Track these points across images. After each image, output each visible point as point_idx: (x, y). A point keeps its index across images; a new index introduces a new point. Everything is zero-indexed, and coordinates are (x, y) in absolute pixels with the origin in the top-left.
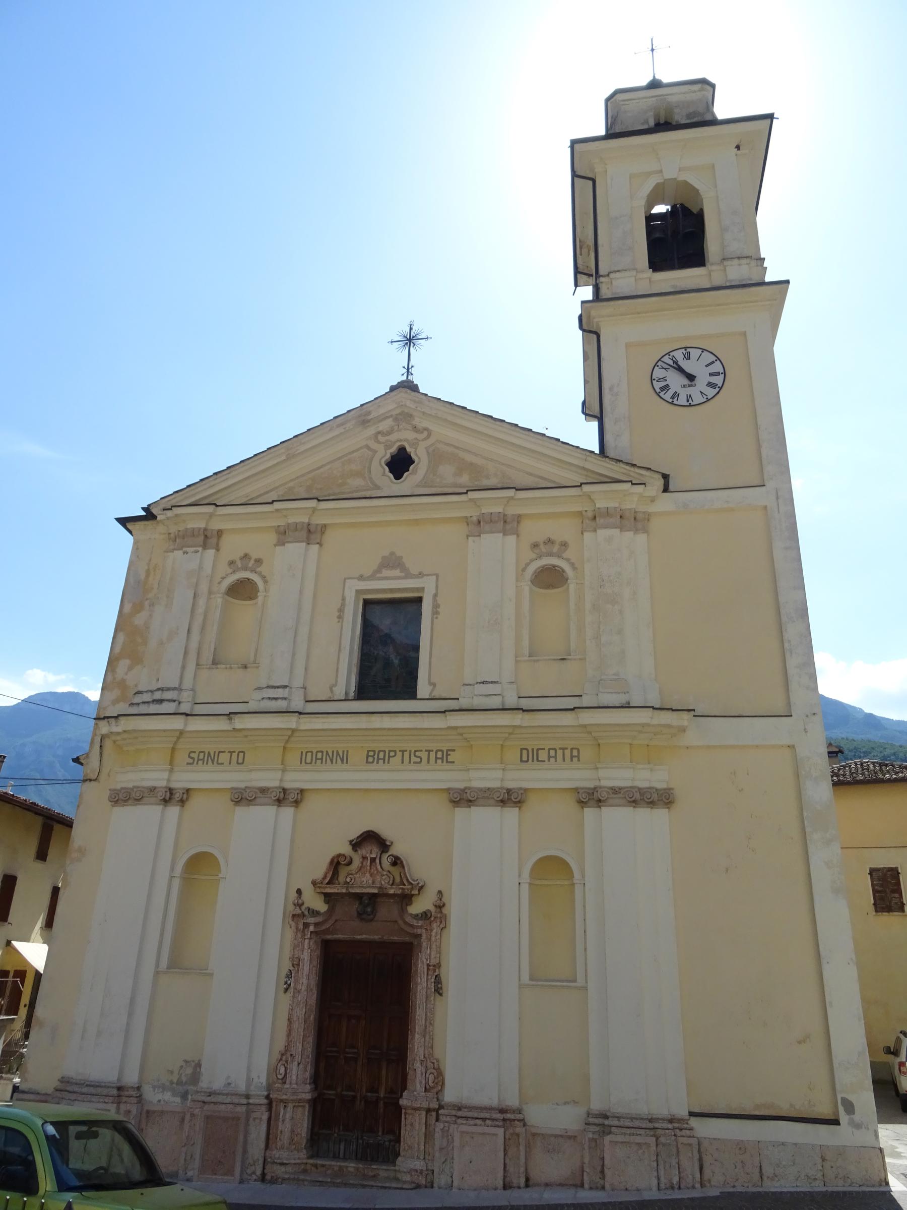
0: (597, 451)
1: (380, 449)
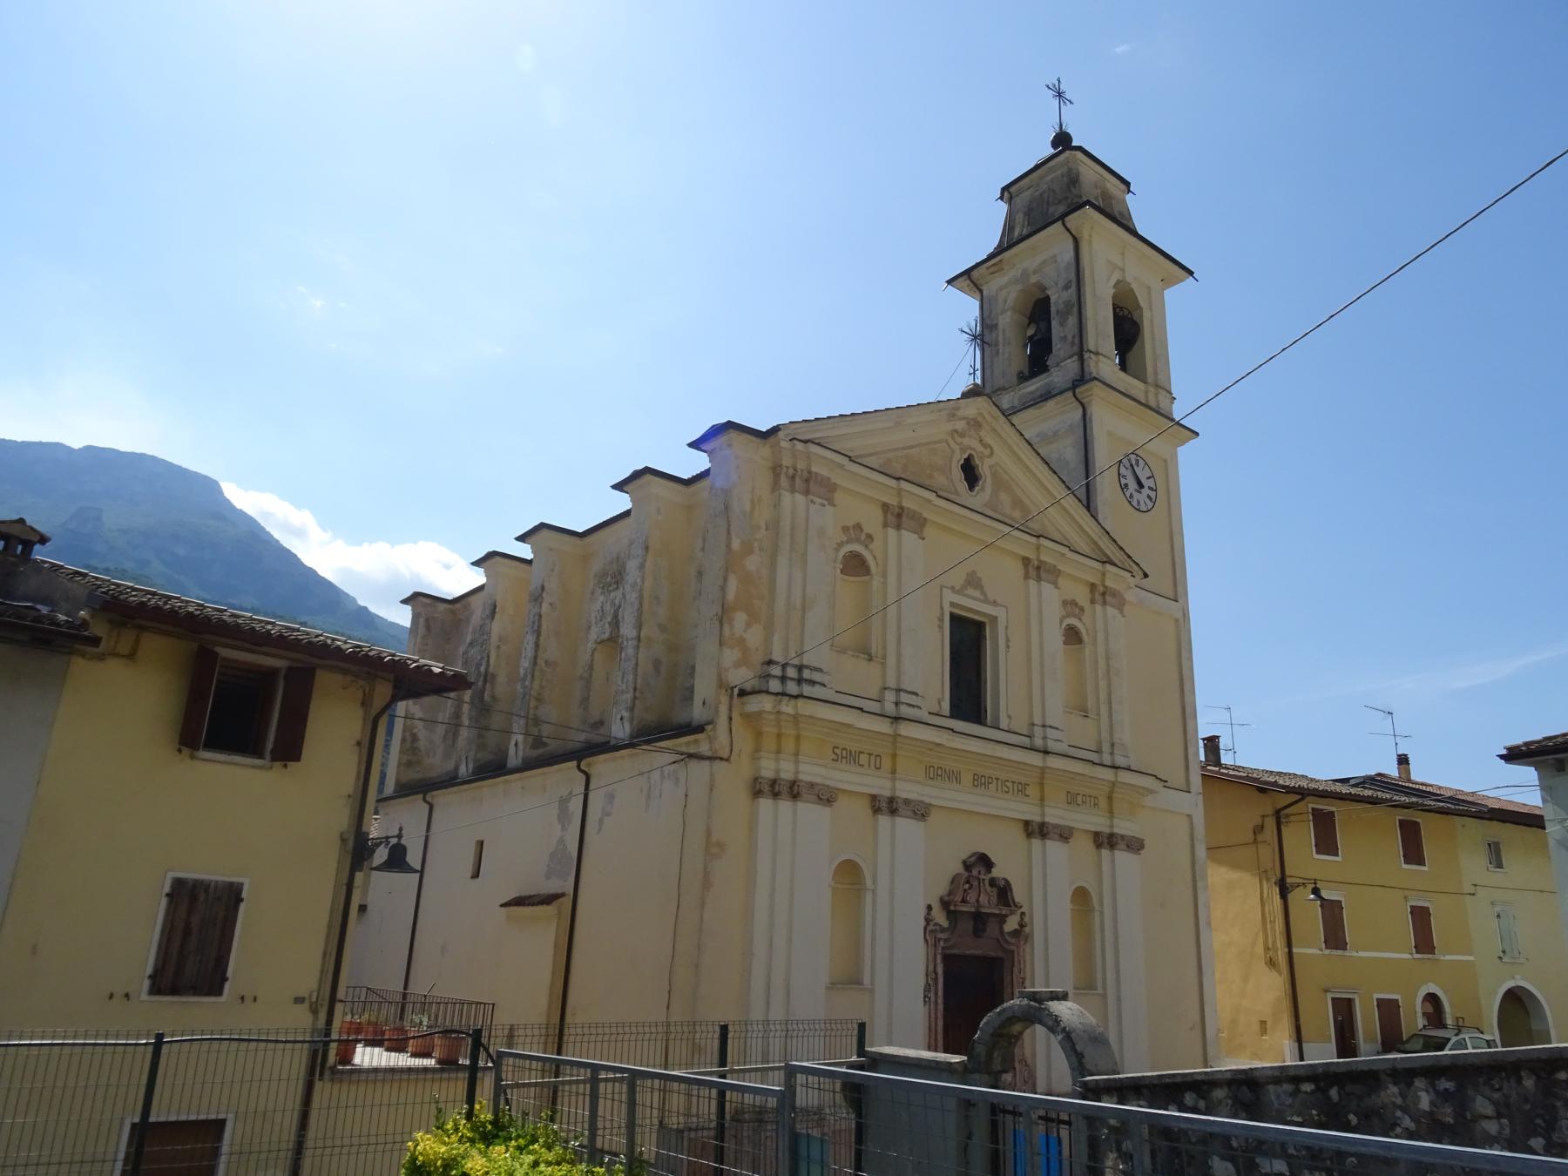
1: (956, 447)
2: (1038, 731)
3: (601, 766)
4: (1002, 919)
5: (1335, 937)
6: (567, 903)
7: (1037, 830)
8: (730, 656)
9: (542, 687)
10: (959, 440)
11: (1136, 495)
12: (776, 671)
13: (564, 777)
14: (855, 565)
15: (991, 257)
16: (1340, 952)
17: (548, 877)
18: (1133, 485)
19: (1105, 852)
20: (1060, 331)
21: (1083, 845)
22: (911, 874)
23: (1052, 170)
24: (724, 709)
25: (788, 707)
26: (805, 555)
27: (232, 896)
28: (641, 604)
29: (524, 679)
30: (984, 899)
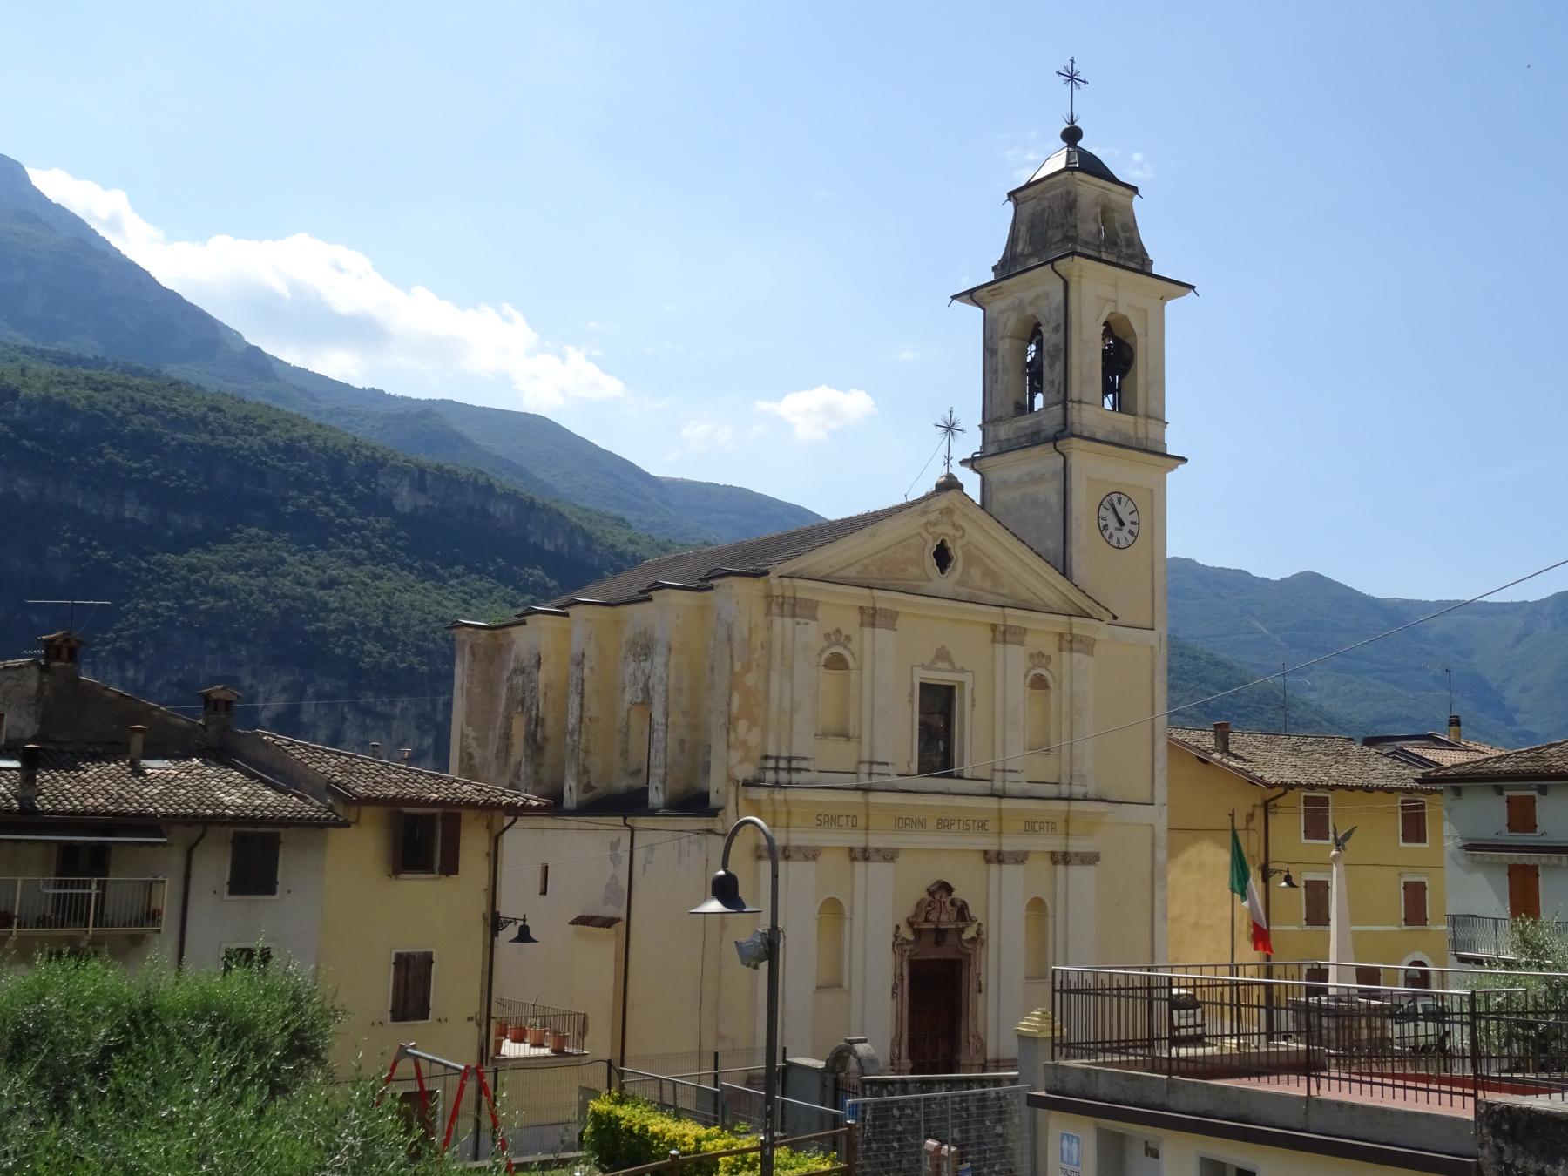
0: (978, 501)
2: (998, 776)
4: (962, 931)
6: (622, 926)
7: (995, 858)
8: (736, 755)
10: (931, 530)
12: (771, 763)
13: (609, 829)
17: (605, 903)
18: (1112, 522)
19: (1060, 868)
21: (1041, 865)
22: (881, 906)
23: (1052, 187)
24: (732, 797)
25: (779, 795)
26: (792, 668)
27: (427, 959)
29: (572, 733)
30: (944, 917)
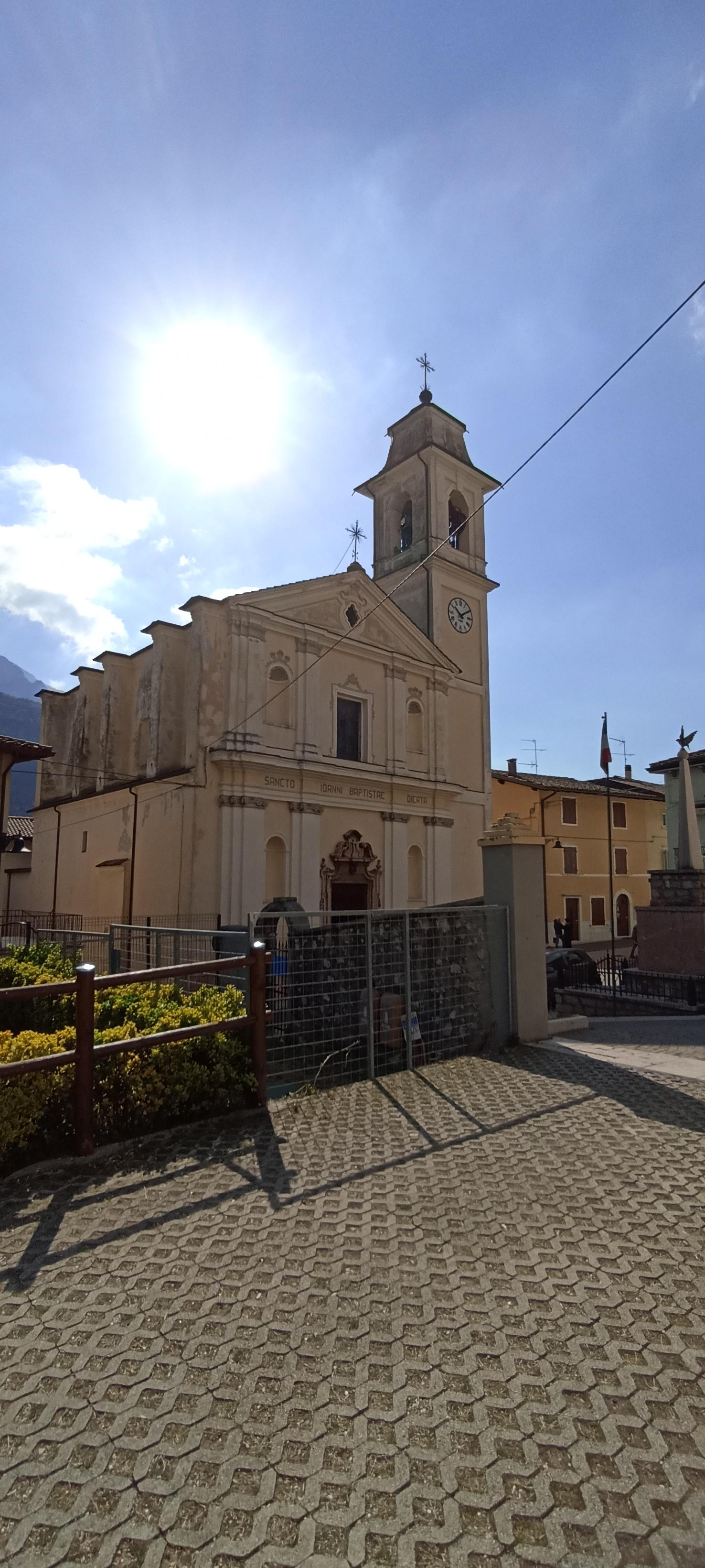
2: (390, 763)
3: (142, 790)
4: (366, 864)
5: (571, 868)
9: (112, 746)
11: (459, 623)
12: (231, 737)
13: (124, 795)
14: (279, 674)
15: (381, 473)
16: (573, 875)
19: (430, 828)
20: (417, 524)
21: (418, 824)
24: (201, 759)
26: (246, 672)
28: (159, 701)
29: (102, 742)
30: (355, 855)
